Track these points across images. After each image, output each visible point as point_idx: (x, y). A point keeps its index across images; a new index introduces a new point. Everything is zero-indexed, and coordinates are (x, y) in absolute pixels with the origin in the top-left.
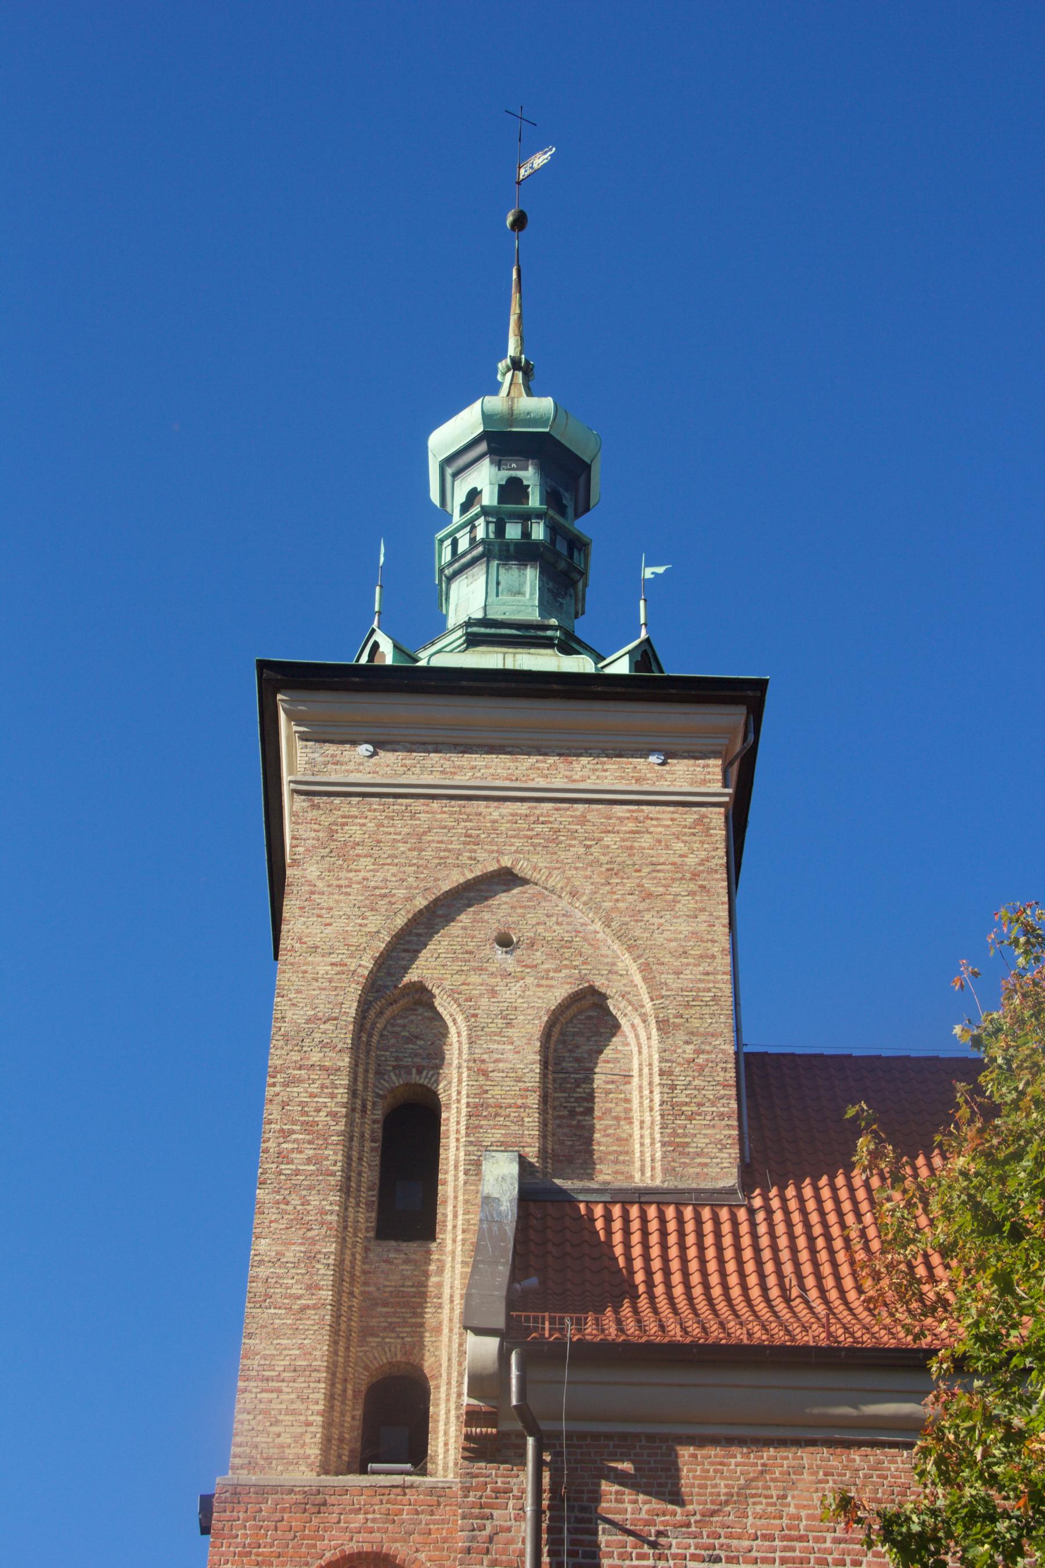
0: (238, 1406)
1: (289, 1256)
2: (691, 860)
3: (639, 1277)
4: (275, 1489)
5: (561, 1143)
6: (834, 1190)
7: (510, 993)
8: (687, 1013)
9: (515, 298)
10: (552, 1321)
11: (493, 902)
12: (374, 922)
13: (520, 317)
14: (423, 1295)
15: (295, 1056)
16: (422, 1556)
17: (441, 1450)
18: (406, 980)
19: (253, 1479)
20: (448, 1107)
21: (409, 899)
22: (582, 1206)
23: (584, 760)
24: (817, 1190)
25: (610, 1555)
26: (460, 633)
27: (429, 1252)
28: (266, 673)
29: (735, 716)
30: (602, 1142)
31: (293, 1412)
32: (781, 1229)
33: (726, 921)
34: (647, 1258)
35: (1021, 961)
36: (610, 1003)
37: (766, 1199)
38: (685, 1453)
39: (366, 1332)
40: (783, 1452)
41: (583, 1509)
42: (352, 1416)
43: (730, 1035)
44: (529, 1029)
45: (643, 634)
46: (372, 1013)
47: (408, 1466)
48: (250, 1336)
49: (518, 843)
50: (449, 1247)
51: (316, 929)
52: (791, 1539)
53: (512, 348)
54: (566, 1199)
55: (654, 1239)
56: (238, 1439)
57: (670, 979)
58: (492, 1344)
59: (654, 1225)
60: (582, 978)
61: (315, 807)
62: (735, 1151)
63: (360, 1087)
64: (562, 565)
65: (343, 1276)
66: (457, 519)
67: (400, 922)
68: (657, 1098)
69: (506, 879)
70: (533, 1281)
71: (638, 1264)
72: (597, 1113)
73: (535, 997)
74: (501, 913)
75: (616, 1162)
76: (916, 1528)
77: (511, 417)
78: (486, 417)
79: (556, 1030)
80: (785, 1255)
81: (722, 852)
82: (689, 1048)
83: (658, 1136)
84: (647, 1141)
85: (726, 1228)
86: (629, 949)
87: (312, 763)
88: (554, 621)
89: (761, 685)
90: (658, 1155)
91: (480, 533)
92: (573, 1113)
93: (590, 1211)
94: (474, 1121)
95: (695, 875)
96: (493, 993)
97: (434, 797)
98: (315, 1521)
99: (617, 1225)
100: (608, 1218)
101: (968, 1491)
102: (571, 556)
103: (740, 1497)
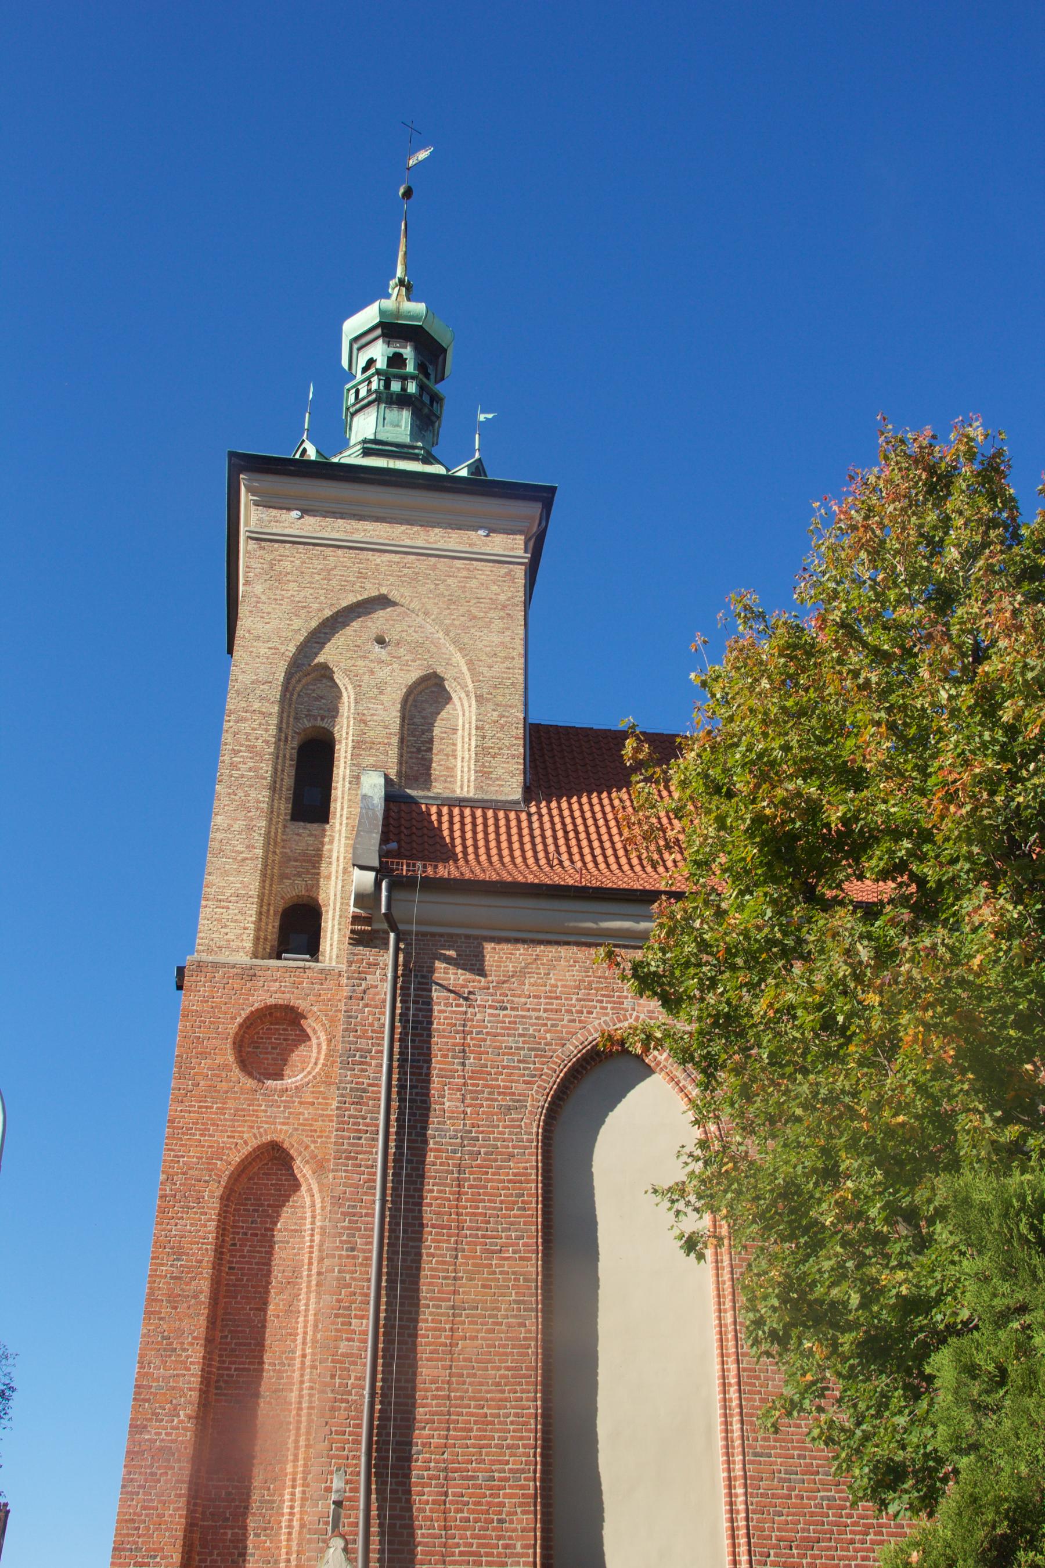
0: (201, 916)
1: (236, 827)
2: (502, 597)
3: (459, 849)
4: (224, 965)
5: (411, 768)
6: (581, 805)
7: (383, 673)
8: (495, 692)
9: (403, 241)
10: (408, 865)
11: (374, 616)
12: (297, 623)
13: (405, 253)
14: (320, 856)
15: (243, 704)
16: (315, 1009)
17: (328, 948)
18: (316, 661)
19: (210, 958)
20: (340, 742)
21: (321, 610)
22: (423, 807)
23: (437, 530)
24: (570, 804)
25: (439, 1004)
26: (359, 447)
27: (324, 830)
28: (234, 460)
29: (534, 509)
30: (437, 769)
31: (236, 921)
32: (547, 826)
33: (522, 636)
34: (463, 838)
35: (741, 628)
36: (446, 684)
37: (539, 808)
38: (488, 947)
39: (283, 876)
40: (550, 948)
41: (423, 977)
42: (273, 926)
43: (521, 707)
44: (394, 696)
45: (477, 455)
46: (294, 681)
47: (308, 957)
48: (210, 874)
49: (392, 579)
50: (337, 828)
51: (260, 625)
52: (551, 998)
53: (400, 272)
54: (413, 801)
55: (468, 827)
56: (201, 935)
57: (485, 670)
58: (371, 875)
59: (468, 820)
60: (429, 666)
61: (262, 548)
62: (521, 778)
63: (284, 726)
64: (426, 411)
65: (269, 841)
66: (359, 377)
67: (314, 624)
68: (473, 743)
69: (383, 602)
70: (393, 846)
71: (458, 841)
72: (435, 751)
73: (399, 678)
74: (379, 623)
75: (446, 782)
76: (653, 969)
77: (398, 314)
78: (382, 313)
79: (411, 698)
80: (550, 841)
81: (522, 594)
82: (495, 714)
83: (472, 767)
84: (466, 769)
85: (513, 823)
86: (461, 650)
87: (260, 520)
88: (420, 444)
89: (553, 490)
90: (472, 778)
91: (374, 386)
92: (419, 750)
93: (428, 809)
94: (356, 751)
95: (504, 607)
96: (372, 672)
97: (339, 547)
98: (249, 985)
99: (445, 818)
100: (440, 814)
101: (687, 949)
102: (432, 405)
103: (521, 973)
